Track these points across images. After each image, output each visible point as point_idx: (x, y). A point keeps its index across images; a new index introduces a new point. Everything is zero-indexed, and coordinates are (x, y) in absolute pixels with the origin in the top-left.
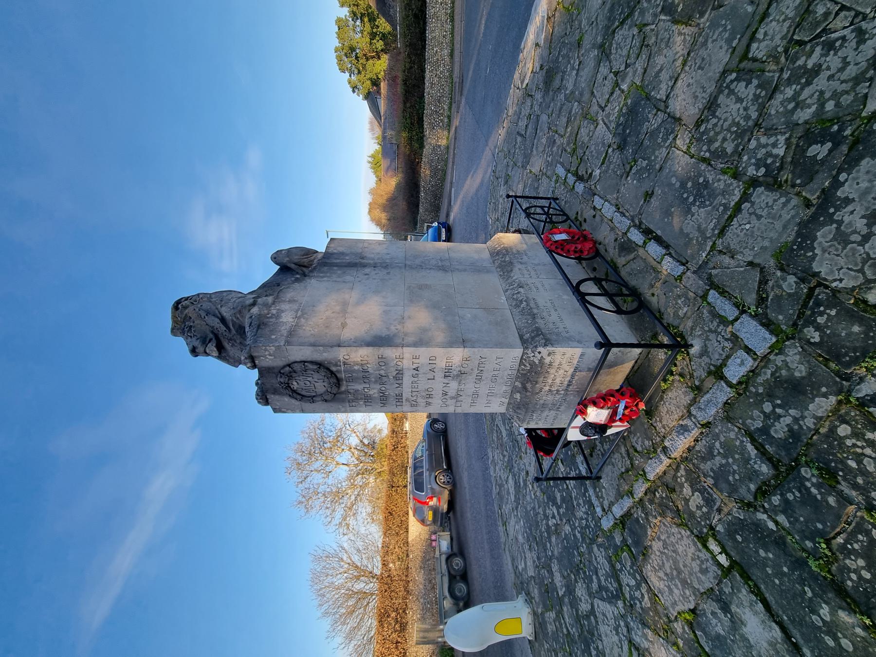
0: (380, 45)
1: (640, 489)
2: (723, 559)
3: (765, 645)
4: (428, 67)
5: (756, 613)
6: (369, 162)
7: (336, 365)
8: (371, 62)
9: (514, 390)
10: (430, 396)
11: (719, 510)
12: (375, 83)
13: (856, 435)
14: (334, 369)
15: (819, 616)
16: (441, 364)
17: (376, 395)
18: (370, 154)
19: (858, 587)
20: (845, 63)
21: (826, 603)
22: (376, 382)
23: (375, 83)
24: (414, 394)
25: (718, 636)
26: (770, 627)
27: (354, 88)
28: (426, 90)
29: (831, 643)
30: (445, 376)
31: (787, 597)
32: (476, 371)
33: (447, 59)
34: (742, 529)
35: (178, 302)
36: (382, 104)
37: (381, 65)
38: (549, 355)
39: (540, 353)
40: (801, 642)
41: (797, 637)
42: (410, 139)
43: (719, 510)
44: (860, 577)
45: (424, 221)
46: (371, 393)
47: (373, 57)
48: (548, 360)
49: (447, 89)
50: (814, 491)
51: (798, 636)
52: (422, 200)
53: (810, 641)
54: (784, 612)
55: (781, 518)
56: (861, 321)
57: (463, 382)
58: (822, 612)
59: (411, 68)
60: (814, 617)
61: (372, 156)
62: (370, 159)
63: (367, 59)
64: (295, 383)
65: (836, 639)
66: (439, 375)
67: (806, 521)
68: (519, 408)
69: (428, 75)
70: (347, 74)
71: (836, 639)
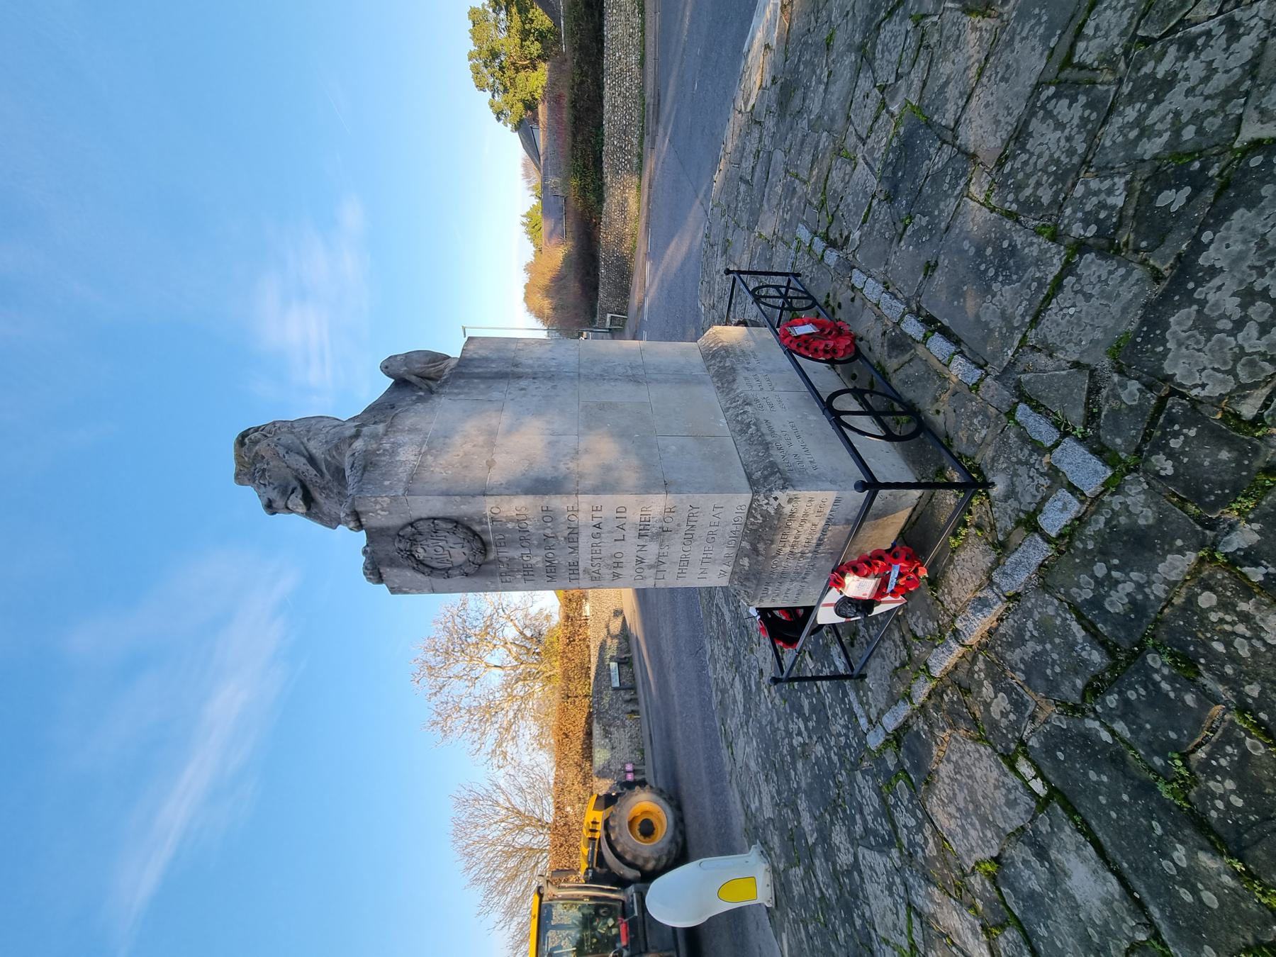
1: (921, 690)
2: (1038, 786)
3: (1098, 903)
4: (607, 81)
5: (1085, 861)
6: (524, 224)
7: (481, 523)
8: (522, 74)
9: (740, 553)
10: (618, 565)
11: (1033, 718)
12: (530, 106)
13: (1225, 605)
14: (477, 528)
15: (1172, 860)
16: (634, 516)
17: (540, 565)
18: (524, 213)
19: (1225, 819)
20: (1211, 71)
21: (1182, 842)
22: (539, 546)
23: (530, 106)
24: (596, 562)
25: (1032, 894)
26: (1104, 878)
27: (499, 114)
28: (606, 116)
29: (1188, 898)
31: (1127, 836)
33: (635, 69)
34: (1065, 743)
35: (244, 435)
36: (541, 138)
37: (538, 79)
38: (790, 501)
39: (776, 499)
40: (1146, 897)
41: (1141, 892)
42: (583, 189)
43: (1033, 718)
44: (1228, 805)
45: (606, 311)
46: (533, 561)
48: (788, 509)
49: (635, 114)
50: (1165, 686)
51: (1143, 890)
52: (603, 279)
53: (1160, 895)
54: (1123, 856)
55: (1120, 726)
56: (1230, 443)
58: (1175, 855)
59: (582, 82)
60: (1164, 863)
61: (528, 215)
62: (524, 220)
64: (420, 550)
65: (1195, 892)
66: (631, 534)
67: (1154, 729)
68: (747, 579)
69: (607, 92)
70: (489, 94)
71: (1195, 892)
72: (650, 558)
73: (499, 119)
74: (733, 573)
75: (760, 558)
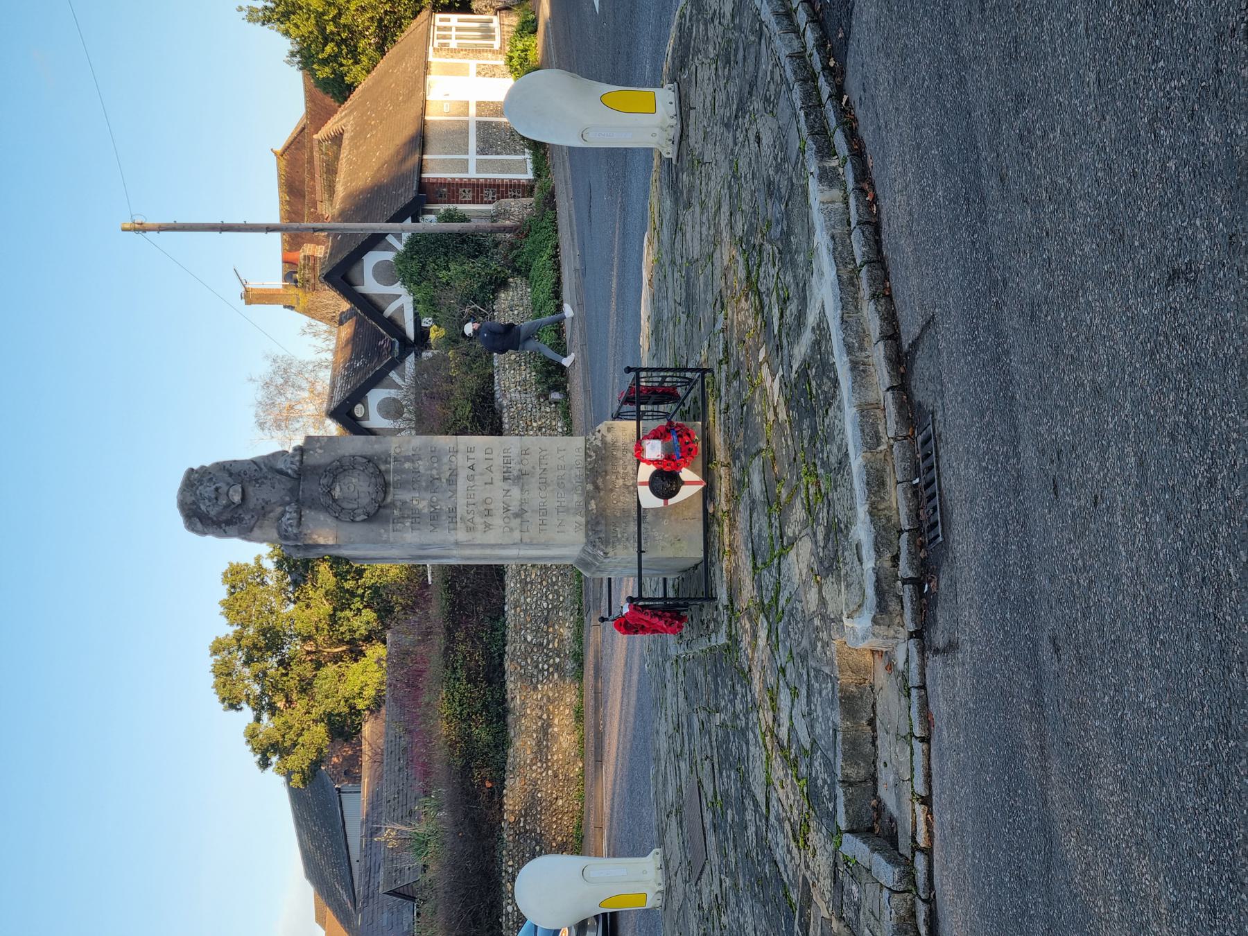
0: (362, 620)
7: (386, 462)
8: (330, 669)
9: (588, 497)
10: (488, 513)
12: (343, 728)
14: (383, 467)
17: (426, 511)
23: (343, 728)
24: (471, 507)
27: (267, 751)
28: (510, 598)
30: (505, 479)
32: (538, 471)
36: (357, 806)
37: (366, 675)
38: (609, 430)
46: (420, 506)
47: (337, 659)
48: (609, 438)
57: (526, 487)
63: (319, 665)
66: (498, 476)
68: (598, 523)
72: (514, 507)
73: (264, 764)
74: (587, 523)
75: (602, 493)
